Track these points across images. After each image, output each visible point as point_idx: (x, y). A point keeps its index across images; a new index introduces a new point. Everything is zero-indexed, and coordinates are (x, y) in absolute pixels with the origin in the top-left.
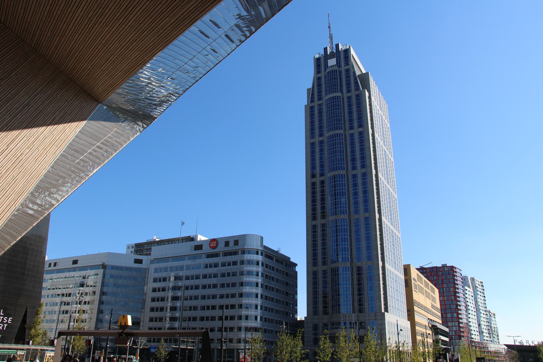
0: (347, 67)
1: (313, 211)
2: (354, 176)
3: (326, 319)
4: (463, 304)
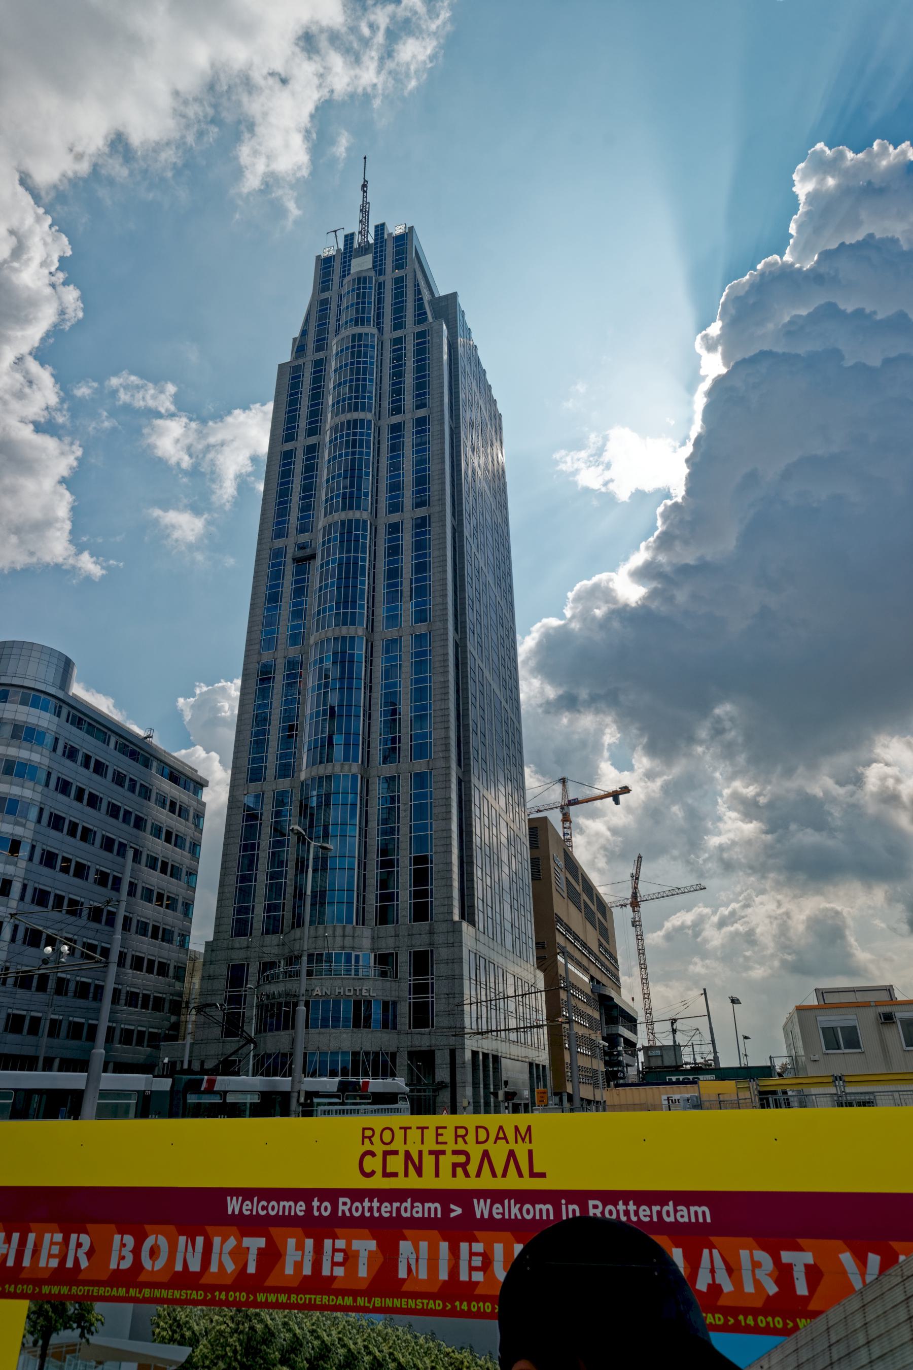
2: (395, 528)
3: (272, 946)
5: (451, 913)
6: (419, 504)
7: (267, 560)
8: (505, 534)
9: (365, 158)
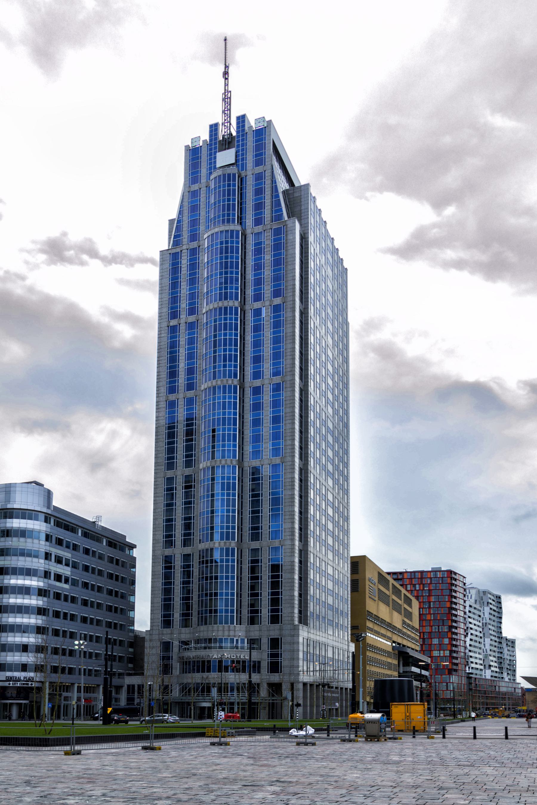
0: (259, 169)
1: (169, 437)
3: (186, 634)
4: (462, 625)
5: (293, 620)
6: (276, 373)
7: (164, 409)
8: (344, 307)
9: (225, 40)
